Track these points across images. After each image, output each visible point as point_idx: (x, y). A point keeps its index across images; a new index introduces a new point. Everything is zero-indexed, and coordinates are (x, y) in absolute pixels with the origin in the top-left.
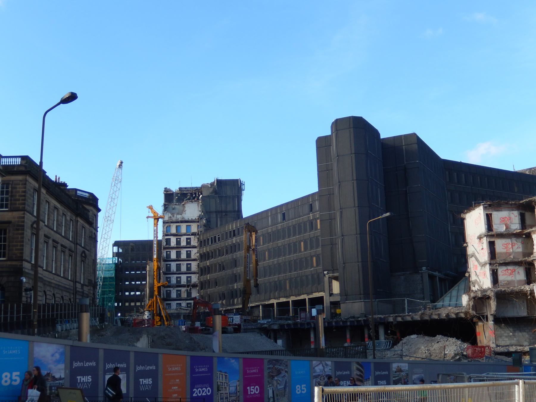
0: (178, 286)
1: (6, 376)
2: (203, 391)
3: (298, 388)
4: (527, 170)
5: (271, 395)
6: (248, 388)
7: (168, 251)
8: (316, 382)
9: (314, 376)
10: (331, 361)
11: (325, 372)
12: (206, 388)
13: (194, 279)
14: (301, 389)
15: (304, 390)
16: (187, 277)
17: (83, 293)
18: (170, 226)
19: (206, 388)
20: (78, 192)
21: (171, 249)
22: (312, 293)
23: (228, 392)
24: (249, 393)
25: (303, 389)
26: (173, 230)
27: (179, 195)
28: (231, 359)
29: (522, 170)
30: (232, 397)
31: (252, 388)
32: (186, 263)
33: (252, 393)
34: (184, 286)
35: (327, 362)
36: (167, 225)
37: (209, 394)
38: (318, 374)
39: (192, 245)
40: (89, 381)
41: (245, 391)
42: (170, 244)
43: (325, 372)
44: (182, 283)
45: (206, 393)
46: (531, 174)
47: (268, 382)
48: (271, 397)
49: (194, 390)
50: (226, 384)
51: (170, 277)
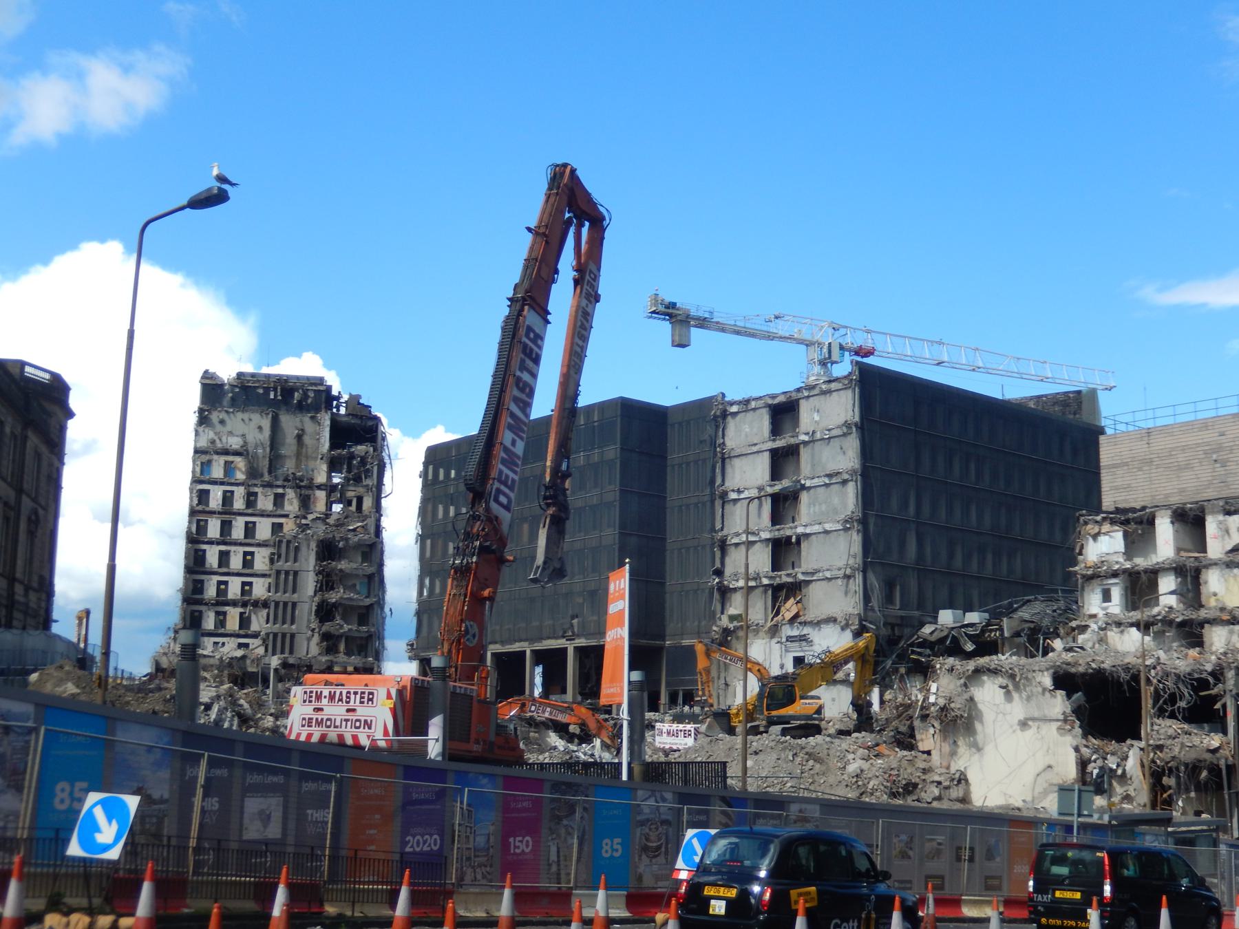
0: (218, 603)
1: (63, 790)
2: (425, 842)
3: (607, 844)
4: (1032, 398)
5: (553, 857)
6: (511, 840)
7: (202, 520)
8: (641, 834)
9: (639, 821)
10: (674, 793)
11: (660, 814)
12: (431, 835)
13: (260, 589)
14: (71, 793)
15: (617, 850)
16: (244, 584)
17: (27, 605)
18: (210, 462)
19: (431, 835)
20: (27, 369)
21: (208, 515)
22: (541, 639)
23: (471, 846)
24: (512, 851)
25: (615, 847)
26: (217, 472)
27: (237, 390)
28: (481, 777)
29: (1022, 399)
30: (478, 856)
31: (519, 841)
32: (241, 549)
33: (518, 851)
34: (234, 603)
35: (664, 794)
36: (205, 458)
37: (435, 848)
38: (646, 817)
39: (258, 508)
40: (213, 808)
41: (505, 846)
42: (207, 505)
43: (660, 814)
44: (230, 596)
45: (430, 845)
46: (1040, 408)
47: (550, 829)
48: (553, 861)
49: (407, 839)
50: (468, 829)
51: (203, 580)
